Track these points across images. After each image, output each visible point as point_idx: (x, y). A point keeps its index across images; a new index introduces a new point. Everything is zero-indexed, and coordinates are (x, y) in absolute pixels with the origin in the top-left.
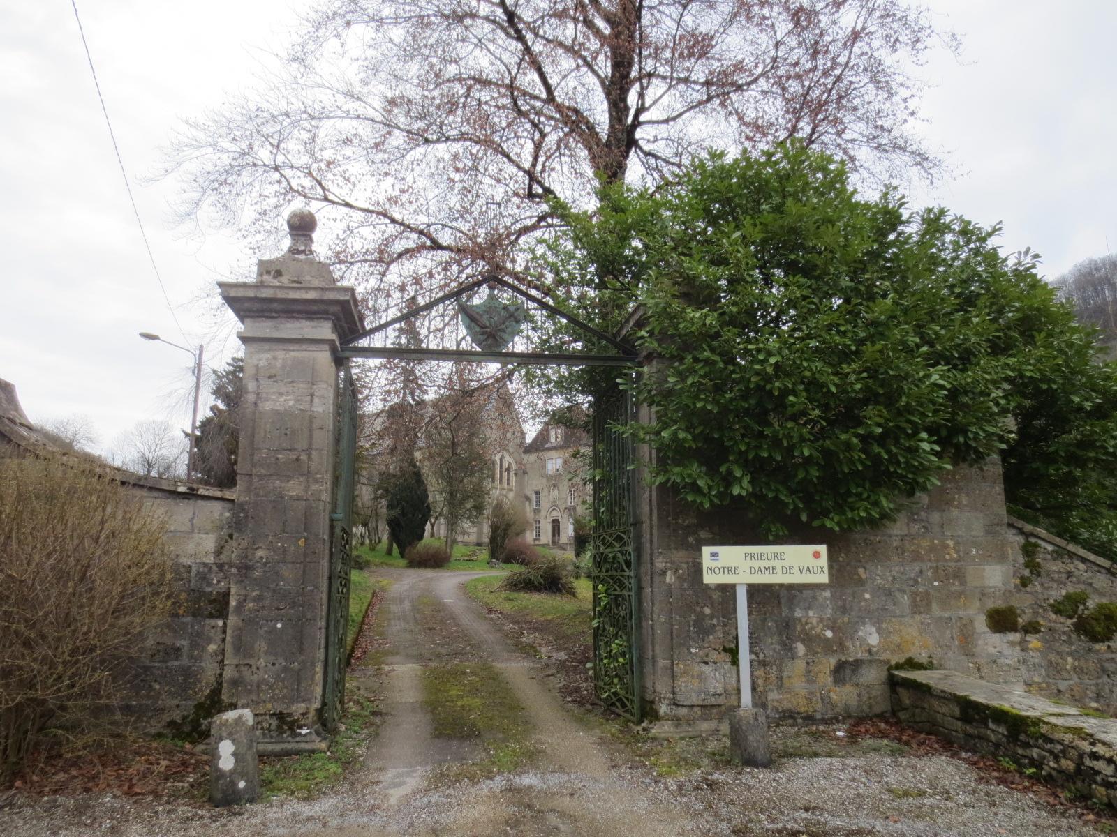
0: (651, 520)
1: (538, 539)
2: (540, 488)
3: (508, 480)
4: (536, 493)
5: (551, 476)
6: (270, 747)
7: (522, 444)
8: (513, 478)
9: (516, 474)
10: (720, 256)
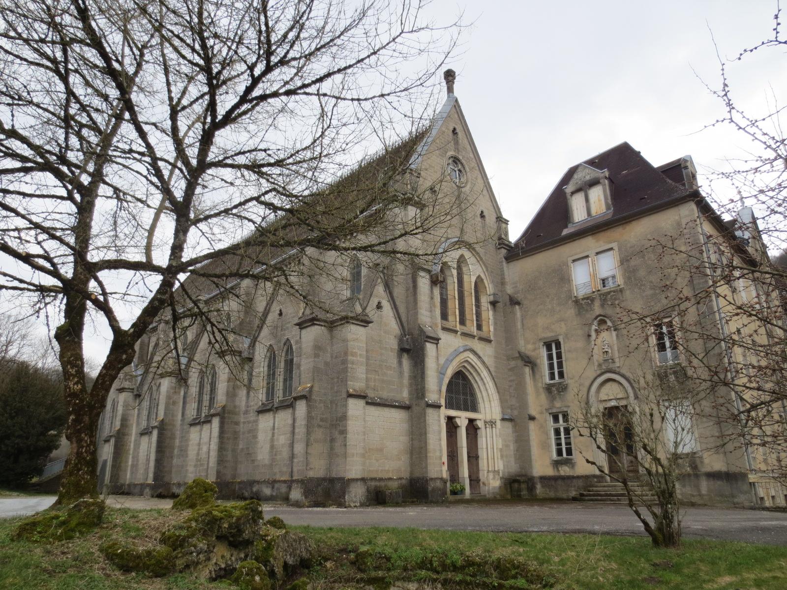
0: (184, 57)
1: (569, 462)
2: (559, 330)
3: (478, 315)
4: (549, 347)
5: (589, 299)
6: (208, 296)
7: (502, 241)
8: (488, 314)
9: (494, 304)
10: (255, 161)
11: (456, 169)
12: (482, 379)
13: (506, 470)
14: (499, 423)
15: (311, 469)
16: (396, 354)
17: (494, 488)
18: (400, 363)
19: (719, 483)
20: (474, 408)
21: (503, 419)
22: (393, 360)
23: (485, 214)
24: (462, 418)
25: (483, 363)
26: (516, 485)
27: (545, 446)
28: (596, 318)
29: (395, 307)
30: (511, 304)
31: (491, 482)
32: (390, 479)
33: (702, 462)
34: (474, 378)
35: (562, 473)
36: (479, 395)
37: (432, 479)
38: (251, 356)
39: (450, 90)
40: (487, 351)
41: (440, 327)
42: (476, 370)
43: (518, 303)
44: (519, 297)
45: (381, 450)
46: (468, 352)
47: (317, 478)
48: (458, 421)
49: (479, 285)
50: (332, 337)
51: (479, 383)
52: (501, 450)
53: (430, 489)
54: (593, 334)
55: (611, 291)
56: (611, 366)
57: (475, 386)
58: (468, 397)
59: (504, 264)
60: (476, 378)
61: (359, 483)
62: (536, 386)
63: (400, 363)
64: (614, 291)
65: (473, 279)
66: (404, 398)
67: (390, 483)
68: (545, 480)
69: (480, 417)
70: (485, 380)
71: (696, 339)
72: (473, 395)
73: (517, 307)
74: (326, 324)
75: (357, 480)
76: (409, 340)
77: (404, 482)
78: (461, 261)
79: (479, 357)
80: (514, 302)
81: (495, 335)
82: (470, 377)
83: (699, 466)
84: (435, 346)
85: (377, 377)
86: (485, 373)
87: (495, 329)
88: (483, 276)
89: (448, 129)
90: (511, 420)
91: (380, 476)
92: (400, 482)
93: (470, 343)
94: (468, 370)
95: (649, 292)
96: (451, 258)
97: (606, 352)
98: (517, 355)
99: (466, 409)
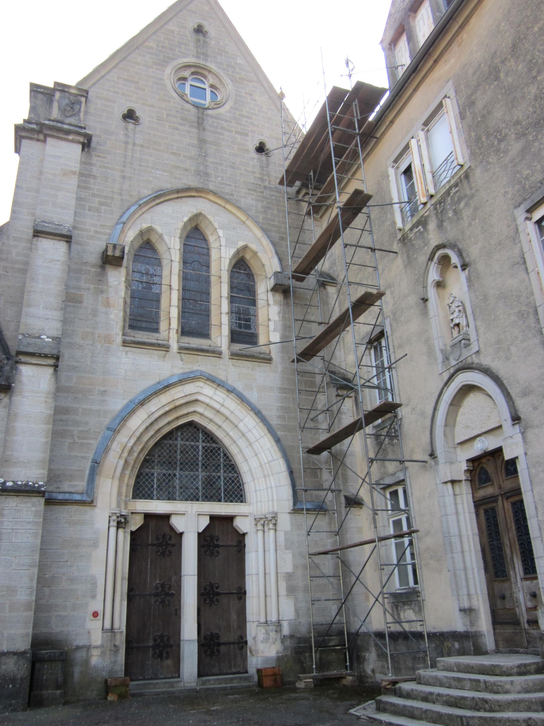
9: (282, 289)
13: (304, 620)
14: (285, 521)
20: (236, 493)
25: (242, 399)
28: (431, 259)
30: (320, 286)
37: (78, 648)
41: (119, 339)
48: (177, 523)
49: (241, 266)
52: (289, 576)
54: (432, 293)
55: (450, 188)
56: (466, 353)
58: (222, 473)
64: (456, 185)
71: (540, 188)
72: (232, 467)
78: (195, 235)
86: (249, 422)
93: (203, 364)
95: (516, 147)
96: (168, 224)
97: (458, 325)
99: (211, 496)
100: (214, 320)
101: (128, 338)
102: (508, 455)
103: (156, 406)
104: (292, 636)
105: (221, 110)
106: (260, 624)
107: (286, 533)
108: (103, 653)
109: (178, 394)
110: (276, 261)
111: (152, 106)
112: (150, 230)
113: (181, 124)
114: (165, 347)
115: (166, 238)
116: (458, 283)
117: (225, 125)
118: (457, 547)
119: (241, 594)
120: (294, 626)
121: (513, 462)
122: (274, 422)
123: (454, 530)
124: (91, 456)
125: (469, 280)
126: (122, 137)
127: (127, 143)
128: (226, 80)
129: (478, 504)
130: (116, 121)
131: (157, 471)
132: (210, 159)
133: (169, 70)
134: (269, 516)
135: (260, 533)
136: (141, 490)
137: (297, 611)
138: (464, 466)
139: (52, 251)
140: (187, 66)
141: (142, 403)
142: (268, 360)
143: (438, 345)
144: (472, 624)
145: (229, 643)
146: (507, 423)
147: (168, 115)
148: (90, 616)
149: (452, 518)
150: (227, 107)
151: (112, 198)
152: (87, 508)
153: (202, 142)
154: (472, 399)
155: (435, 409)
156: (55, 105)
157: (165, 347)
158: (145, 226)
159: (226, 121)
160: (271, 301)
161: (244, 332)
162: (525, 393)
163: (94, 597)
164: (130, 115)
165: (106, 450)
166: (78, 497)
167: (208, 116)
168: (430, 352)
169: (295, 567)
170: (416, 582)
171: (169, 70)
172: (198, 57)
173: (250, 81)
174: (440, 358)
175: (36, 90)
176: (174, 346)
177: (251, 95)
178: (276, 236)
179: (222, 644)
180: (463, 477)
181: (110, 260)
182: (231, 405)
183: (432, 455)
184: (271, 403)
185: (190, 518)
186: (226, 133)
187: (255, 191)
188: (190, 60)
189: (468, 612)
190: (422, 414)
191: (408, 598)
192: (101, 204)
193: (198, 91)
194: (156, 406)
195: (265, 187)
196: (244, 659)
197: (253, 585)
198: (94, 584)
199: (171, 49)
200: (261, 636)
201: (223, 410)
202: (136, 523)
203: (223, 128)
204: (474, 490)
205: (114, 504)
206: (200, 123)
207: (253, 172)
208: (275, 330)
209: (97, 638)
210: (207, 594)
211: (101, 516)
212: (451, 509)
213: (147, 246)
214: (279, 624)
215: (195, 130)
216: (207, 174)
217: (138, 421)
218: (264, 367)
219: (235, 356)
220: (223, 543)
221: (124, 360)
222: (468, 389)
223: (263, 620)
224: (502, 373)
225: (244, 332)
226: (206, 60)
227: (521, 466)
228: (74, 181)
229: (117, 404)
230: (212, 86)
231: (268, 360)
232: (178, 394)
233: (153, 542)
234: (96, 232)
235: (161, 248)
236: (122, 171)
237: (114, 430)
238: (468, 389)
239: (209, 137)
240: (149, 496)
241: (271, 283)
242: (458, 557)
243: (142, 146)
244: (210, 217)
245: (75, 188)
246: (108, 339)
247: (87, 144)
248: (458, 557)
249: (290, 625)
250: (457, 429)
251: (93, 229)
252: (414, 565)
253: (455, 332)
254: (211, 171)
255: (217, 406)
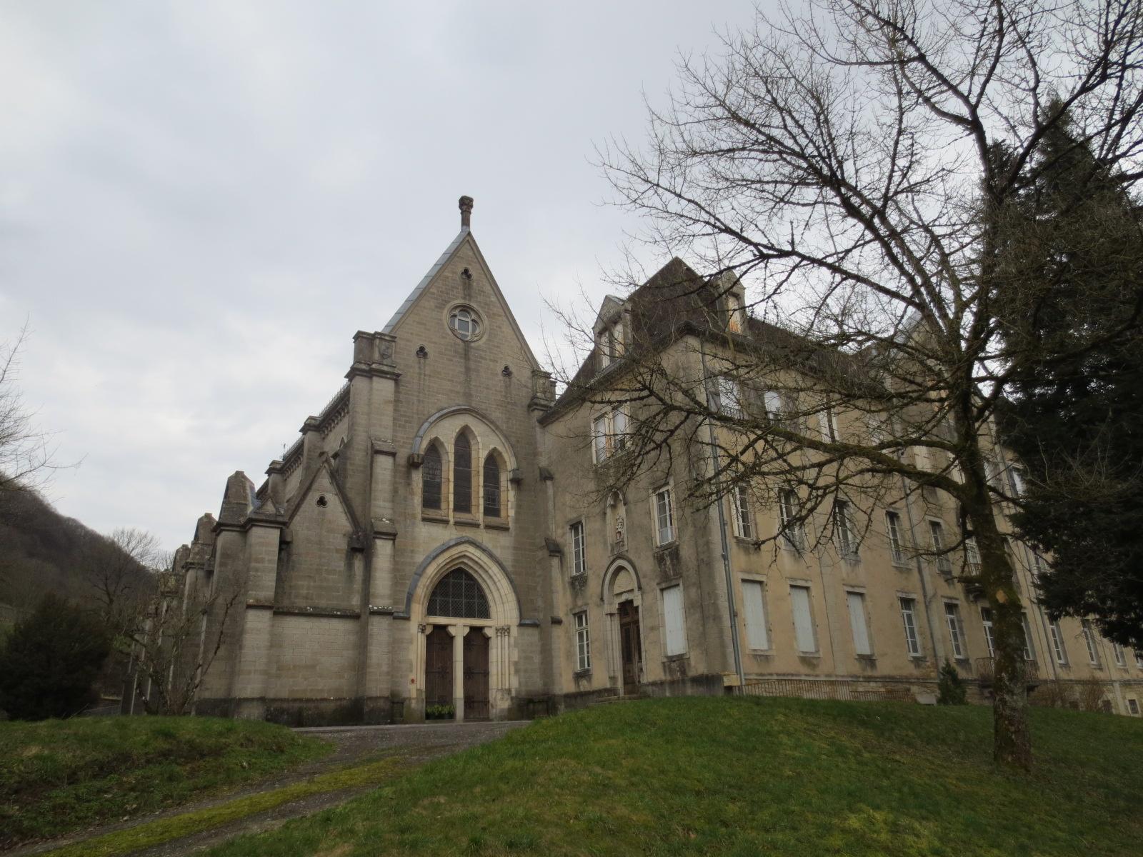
8: (508, 496)
9: (517, 482)
11: (469, 320)
12: (491, 577)
13: (523, 689)
14: (515, 631)
15: (207, 689)
16: (344, 556)
17: (502, 710)
18: (350, 565)
19: (701, 689)
20: (484, 613)
21: (521, 625)
22: (340, 564)
23: (512, 369)
24: (459, 627)
25: (491, 556)
26: (531, 706)
27: (569, 655)
29: (346, 501)
30: (541, 480)
31: (499, 703)
32: (323, 700)
33: (689, 664)
34: (481, 576)
35: (582, 689)
36: (489, 597)
37: (371, 698)
38: (212, 569)
39: (466, 221)
40: (501, 544)
41: (419, 517)
42: (481, 567)
43: (551, 478)
44: (553, 469)
45: (313, 667)
46: (467, 545)
47: (214, 699)
48: (452, 630)
49: (493, 461)
50: (245, 543)
51: (488, 581)
52: (516, 663)
53: (366, 709)
57: (484, 586)
59: (538, 429)
60: (484, 576)
61: (255, 703)
62: (563, 580)
63: (350, 565)
65: (483, 455)
66: (353, 605)
67: (323, 705)
68: (569, 697)
69: (490, 626)
70: (494, 577)
72: (483, 597)
73: (549, 483)
74: (238, 529)
75: (252, 699)
76: (361, 538)
77: (344, 703)
78: (464, 438)
79: (484, 550)
80: (546, 476)
81: (517, 520)
82: (475, 576)
83: (687, 670)
84: (391, 542)
85: (312, 584)
86: (494, 569)
87: (517, 513)
88: (500, 448)
89: (455, 273)
90: (535, 625)
91: (309, 695)
92: (339, 703)
93: (468, 533)
94: (471, 567)
96: (447, 433)
97: (620, 532)
98: (544, 543)
99: (470, 614)
100: (474, 502)
101: (426, 516)
102: (635, 604)
103: (442, 560)
104: (516, 697)
105: (480, 343)
106: (498, 690)
107: (515, 637)
108: (417, 702)
109: (454, 552)
110: (513, 459)
111: (435, 343)
112: (436, 439)
113: (454, 357)
114: (446, 522)
115: (446, 444)
116: (622, 510)
117: (483, 354)
118: (610, 647)
119: (486, 674)
120: (518, 692)
121: (637, 607)
122: (510, 569)
123: (609, 638)
124: (407, 590)
125: (626, 511)
126: (417, 370)
127: (420, 374)
128: (484, 317)
129: (622, 626)
130: (413, 359)
131: (438, 599)
132: (473, 383)
133: (445, 312)
134: (506, 628)
135: (499, 638)
136: (431, 611)
137: (520, 683)
138: (617, 606)
139: (384, 463)
140: (456, 307)
141: (435, 558)
142: (507, 529)
143: (609, 541)
144: (614, 684)
145: (479, 702)
146: (636, 590)
147: (446, 349)
148: (409, 681)
149: (609, 633)
150: (484, 339)
151: (413, 417)
152: (406, 622)
153: (468, 369)
154: (622, 574)
155: (605, 575)
156: (376, 350)
157: (446, 522)
158: (433, 437)
159: (483, 351)
160: (510, 489)
161: (492, 508)
162: (645, 577)
163: (411, 671)
164: (422, 352)
165: (416, 586)
166: (402, 615)
167: (472, 348)
168: (605, 543)
169: (520, 658)
170: (589, 666)
171: (445, 312)
172: (464, 298)
173: (500, 316)
174: (610, 548)
175: (359, 336)
176: (452, 521)
177: (500, 328)
178: (513, 440)
179: (477, 702)
180: (616, 612)
181: (413, 464)
182: (484, 559)
183: (602, 599)
184: (506, 556)
185: (459, 627)
186: (483, 361)
187: (501, 406)
188: (459, 301)
189: (613, 679)
190: (599, 575)
191: (583, 675)
192: (406, 422)
193: (464, 325)
194: (442, 560)
195: (508, 403)
196: (488, 711)
197: (494, 669)
198: (411, 665)
199: (447, 294)
200: (499, 696)
201: (480, 561)
202: (429, 630)
203: (482, 358)
204: (621, 619)
205: (420, 620)
206: (466, 356)
207: (501, 392)
208: (512, 508)
209: (414, 694)
210: (468, 673)
211: (413, 626)
212: (609, 628)
213: (434, 447)
214: (509, 691)
215: (463, 361)
216: (471, 395)
217: (432, 570)
218: (505, 533)
219: (488, 527)
220: (477, 642)
221: (423, 530)
222: (620, 568)
223: (500, 688)
224: (636, 564)
225: (492, 508)
226: (470, 300)
227: (640, 610)
228: (390, 408)
229: (420, 558)
230: (473, 320)
231: (507, 529)
232: (454, 552)
233: (438, 640)
234: (404, 442)
235: (442, 451)
236: (418, 396)
237: (420, 574)
238: (620, 568)
239: (472, 365)
240: (435, 614)
241: (511, 475)
242: (610, 652)
243: (430, 376)
244: (473, 428)
245: (392, 414)
246: (414, 516)
247: (396, 378)
248: (610, 652)
249: (516, 691)
250: (615, 586)
251: (402, 441)
252: (588, 657)
253: (618, 535)
254: (473, 392)
255: (477, 559)
